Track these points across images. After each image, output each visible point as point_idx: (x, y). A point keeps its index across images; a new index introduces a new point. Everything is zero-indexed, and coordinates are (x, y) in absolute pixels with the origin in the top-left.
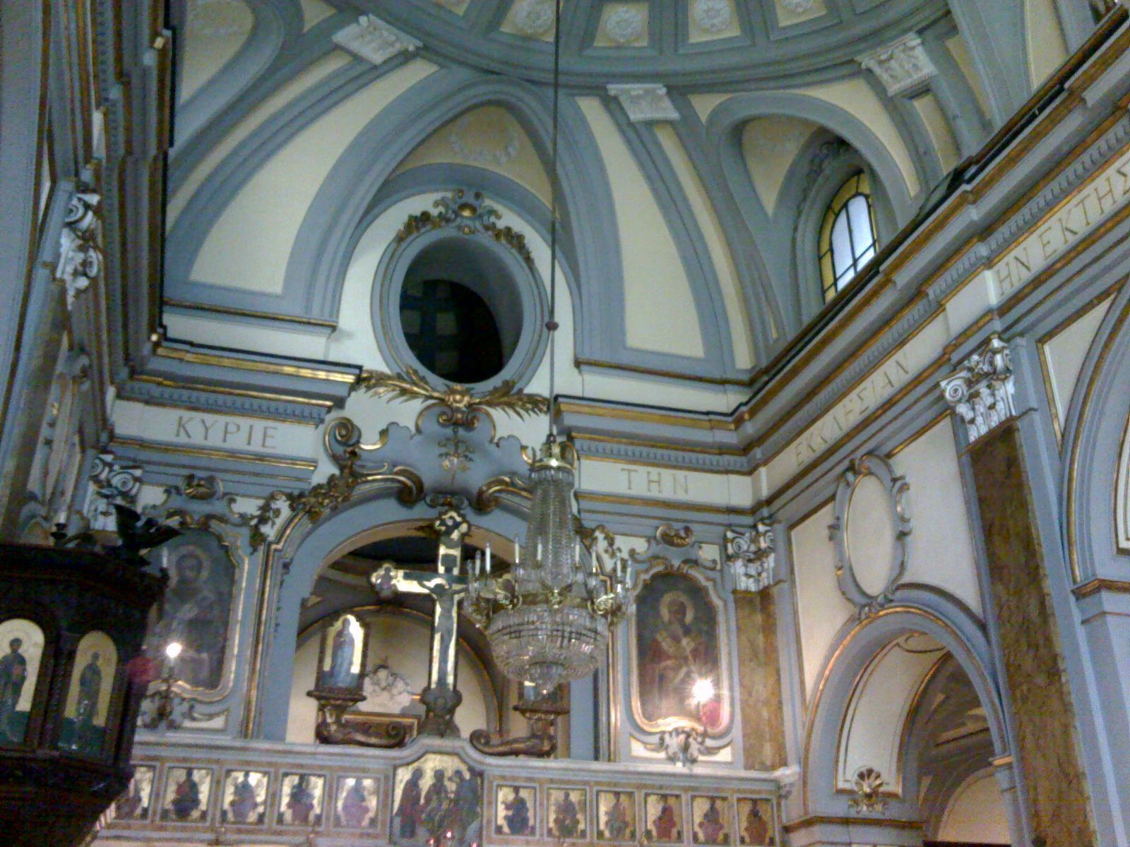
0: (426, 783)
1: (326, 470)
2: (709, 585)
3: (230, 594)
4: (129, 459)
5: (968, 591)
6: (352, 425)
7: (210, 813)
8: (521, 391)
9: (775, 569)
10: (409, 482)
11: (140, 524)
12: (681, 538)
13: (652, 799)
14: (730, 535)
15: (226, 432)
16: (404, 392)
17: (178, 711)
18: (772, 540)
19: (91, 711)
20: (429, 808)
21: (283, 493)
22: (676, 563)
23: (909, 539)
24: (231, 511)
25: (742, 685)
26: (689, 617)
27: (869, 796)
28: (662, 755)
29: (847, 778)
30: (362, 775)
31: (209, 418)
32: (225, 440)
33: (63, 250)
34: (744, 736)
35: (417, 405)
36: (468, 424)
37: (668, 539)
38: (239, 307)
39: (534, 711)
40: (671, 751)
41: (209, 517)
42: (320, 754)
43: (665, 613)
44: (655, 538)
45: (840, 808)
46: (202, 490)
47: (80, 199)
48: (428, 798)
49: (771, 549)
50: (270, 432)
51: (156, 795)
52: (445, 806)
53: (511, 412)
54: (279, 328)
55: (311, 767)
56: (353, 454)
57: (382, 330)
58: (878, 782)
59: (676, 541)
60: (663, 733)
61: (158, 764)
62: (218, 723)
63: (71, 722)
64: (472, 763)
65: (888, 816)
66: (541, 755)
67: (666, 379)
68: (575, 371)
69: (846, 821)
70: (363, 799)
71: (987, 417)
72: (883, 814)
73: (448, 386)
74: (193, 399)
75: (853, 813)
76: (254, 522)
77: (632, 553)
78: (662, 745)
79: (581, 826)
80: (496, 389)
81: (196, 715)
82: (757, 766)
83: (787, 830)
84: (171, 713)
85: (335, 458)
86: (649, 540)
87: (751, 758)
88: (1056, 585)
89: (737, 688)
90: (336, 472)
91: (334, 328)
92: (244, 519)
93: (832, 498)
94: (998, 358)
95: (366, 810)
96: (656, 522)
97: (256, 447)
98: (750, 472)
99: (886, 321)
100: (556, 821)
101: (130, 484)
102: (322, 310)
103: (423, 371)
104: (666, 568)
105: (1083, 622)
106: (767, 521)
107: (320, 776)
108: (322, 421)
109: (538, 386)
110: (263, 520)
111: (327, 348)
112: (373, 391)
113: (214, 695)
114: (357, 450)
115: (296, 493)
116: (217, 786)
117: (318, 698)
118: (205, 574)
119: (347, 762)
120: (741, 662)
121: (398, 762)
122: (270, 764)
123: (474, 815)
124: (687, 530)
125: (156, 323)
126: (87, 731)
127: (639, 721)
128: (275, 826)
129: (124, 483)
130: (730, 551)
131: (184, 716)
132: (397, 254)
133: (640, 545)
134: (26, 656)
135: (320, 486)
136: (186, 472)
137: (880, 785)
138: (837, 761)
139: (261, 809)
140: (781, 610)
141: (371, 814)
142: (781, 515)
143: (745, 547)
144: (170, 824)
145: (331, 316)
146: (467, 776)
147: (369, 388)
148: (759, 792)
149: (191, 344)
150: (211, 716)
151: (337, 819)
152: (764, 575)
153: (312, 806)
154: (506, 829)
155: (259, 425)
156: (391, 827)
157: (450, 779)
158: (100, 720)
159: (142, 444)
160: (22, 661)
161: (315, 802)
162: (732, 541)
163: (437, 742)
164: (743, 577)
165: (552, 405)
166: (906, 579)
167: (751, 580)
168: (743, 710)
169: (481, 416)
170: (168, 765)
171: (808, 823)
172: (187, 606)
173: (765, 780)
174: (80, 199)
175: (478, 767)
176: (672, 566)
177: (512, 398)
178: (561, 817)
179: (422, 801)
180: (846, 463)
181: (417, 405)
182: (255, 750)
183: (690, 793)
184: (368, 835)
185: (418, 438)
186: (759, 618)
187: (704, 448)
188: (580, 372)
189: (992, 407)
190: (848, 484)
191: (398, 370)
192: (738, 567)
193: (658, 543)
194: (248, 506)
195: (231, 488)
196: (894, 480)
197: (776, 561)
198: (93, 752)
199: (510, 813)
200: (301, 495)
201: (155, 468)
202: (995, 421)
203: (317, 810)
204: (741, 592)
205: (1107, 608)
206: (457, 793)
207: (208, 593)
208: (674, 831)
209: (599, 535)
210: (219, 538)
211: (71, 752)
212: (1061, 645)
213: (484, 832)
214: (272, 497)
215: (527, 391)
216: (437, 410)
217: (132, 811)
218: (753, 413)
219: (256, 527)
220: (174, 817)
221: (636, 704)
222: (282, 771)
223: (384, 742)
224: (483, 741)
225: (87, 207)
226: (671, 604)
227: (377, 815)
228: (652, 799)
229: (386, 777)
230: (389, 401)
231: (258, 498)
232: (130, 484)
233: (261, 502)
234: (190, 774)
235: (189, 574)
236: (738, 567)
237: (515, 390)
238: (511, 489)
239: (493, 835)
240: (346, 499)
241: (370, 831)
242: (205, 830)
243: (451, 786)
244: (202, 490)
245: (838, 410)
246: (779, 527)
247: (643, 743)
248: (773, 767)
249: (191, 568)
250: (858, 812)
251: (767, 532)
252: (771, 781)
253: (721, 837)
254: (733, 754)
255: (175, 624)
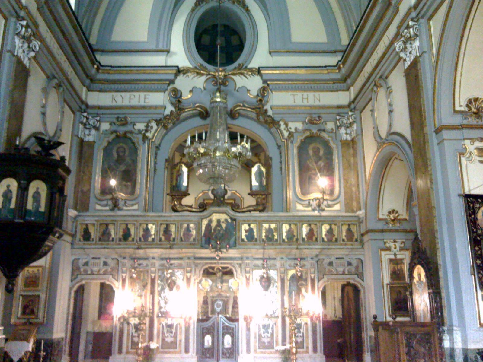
0: (214, 224)
1: (170, 108)
2: (330, 139)
3: (137, 160)
4: (95, 114)
5: (408, 134)
6: (177, 90)
7: (197, 238)
8: (246, 67)
9: (356, 130)
10: (202, 110)
11: (46, 142)
12: (316, 120)
13: (305, 226)
14: (338, 117)
15: (130, 99)
16: (198, 74)
17: (121, 203)
18: (355, 118)
19: (39, 206)
20: (215, 233)
21: (153, 120)
22: (315, 131)
23: (393, 113)
24: (134, 128)
25: (344, 179)
26: (321, 153)
27: (393, 220)
28: (310, 209)
29: (383, 214)
30: (189, 223)
31: (123, 94)
32: (130, 102)
33: (17, 44)
34: (345, 199)
35: (204, 78)
36: (224, 84)
37: (311, 122)
38: (130, 49)
39: (256, 195)
40: (313, 207)
41: (126, 133)
42: (173, 216)
43: (311, 152)
44: (306, 122)
45: (380, 226)
46: (122, 122)
47: (19, 24)
48: (215, 230)
49: (354, 122)
50: (147, 97)
51: (116, 233)
52: (222, 232)
53: (242, 76)
54: (153, 55)
55: (170, 221)
56: (179, 101)
57: (187, 49)
58: (397, 215)
59: (315, 122)
60: (310, 200)
61: (116, 223)
62: (136, 207)
63: (30, 211)
64: (231, 216)
65: (395, 228)
66: (260, 211)
67: (307, 54)
68: (270, 55)
69: (382, 231)
70: (190, 231)
71: (410, 57)
72: (399, 227)
73: (215, 69)
74: (110, 88)
75: (385, 227)
76: (143, 132)
77: (296, 129)
78: (309, 205)
79: (276, 237)
80: (235, 68)
81: (127, 205)
82: (350, 211)
83: (362, 235)
84: (118, 205)
85: (172, 104)
86: (304, 122)
87: (348, 207)
88: (429, 130)
89: (342, 181)
90: (173, 109)
91: (168, 52)
92: (140, 131)
93: (371, 99)
94: (411, 30)
95: (192, 235)
96: (305, 115)
97: (142, 103)
98: (348, 89)
99: (380, 18)
100: (266, 236)
101: (96, 123)
102: (163, 45)
103: (205, 64)
104: (310, 134)
105: (438, 144)
106: (353, 110)
107: (173, 224)
108: (167, 90)
109: (254, 64)
110: (146, 131)
111: (166, 60)
112: (185, 75)
113: (133, 197)
114: (180, 100)
115: (158, 119)
116: (137, 229)
117: (171, 196)
118: (127, 153)
119: (184, 218)
120: (344, 169)
121: (203, 217)
122: (155, 221)
123: (232, 235)
124: (319, 117)
125: (94, 61)
126: (37, 212)
127: (299, 196)
128: (159, 242)
129: (94, 123)
130: (338, 124)
131: (123, 205)
132: (192, 16)
133: (300, 126)
134: (12, 190)
135: (167, 115)
136: (116, 116)
137: (399, 216)
138: (378, 208)
139: (153, 237)
140: (359, 146)
141: (194, 237)
142: (357, 107)
143: (345, 122)
144: (121, 243)
145: (167, 47)
146: (230, 221)
147: (184, 74)
148: (351, 221)
149: (111, 67)
150: (132, 205)
151: (181, 238)
152: (353, 133)
153: (171, 235)
154: (246, 240)
155: (142, 94)
156: (201, 241)
157: (223, 222)
158: (42, 209)
159: (99, 108)
160: (11, 192)
161: (173, 233)
162: (339, 120)
163: (217, 209)
164: (344, 134)
165: (258, 71)
166: (393, 130)
167: (348, 136)
168: (344, 188)
169: (229, 80)
170: (119, 223)
171: (368, 232)
172: (121, 166)
173: (352, 216)
174: (19, 24)
175: (234, 217)
176: (313, 133)
177: (242, 70)
178: (267, 234)
179: (213, 231)
180: (373, 84)
181: (204, 78)
182: (148, 216)
183: (321, 223)
184: (193, 244)
185: (205, 92)
186: (351, 151)
187: (326, 81)
188: (272, 56)
189: (410, 53)
190: (375, 91)
191: (195, 65)
192: (343, 130)
193: (307, 124)
194: (141, 126)
195: (133, 120)
196: (388, 88)
197: (357, 127)
198: (41, 220)
199: (247, 234)
200: (161, 120)
201: (104, 116)
202: (412, 58)
203: (173, 236)
204: (344, 140)
205: (445, 137)
206: (226, 227)
207: (128, 160)
208: (314, 238)
209: (282, 123)
210: (130, 139)
211: (32, 220)
212: (429, 154)
213: (237, 241)
214: (149, 122)
215: (249, 67)
216: (212, 79)
217: (109, 238)
218: (344, 64)
219: (144, 134)
220: (123, 240)
221: (298, 189)
222: (160, 223)
223: (198, 210)
224: (236, 207)
225: (22, 26)
226: (314, 148)
227: (196, 237)
228: (305, 226)
229: (199, 223)
230: (192, 78)
231: (144, 122)
232: (96, 123)
233: (145, 124)
234: (147, 225)
235: (121, 154)
236: (343, 130)
237: (244, 67)
238: (243, 108)
239: (241, 243)
240: (178, 119)
241: (194, 243)
242: (135, 244)
243: (224, 225)
244: (122, 122)
245: (371, 60)
246: (357, 112)
247: (301, 204)
248: (357, 211)
249: (122, 152)
250: (388, 227)
251: (352, 115)
252: (355, 216)
253: (334, 239)
254: (340, 207)
255: (117, 173)
